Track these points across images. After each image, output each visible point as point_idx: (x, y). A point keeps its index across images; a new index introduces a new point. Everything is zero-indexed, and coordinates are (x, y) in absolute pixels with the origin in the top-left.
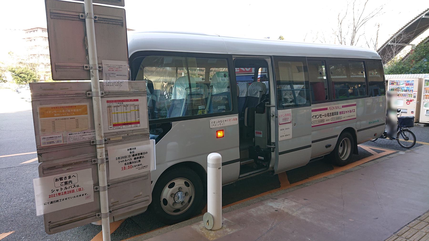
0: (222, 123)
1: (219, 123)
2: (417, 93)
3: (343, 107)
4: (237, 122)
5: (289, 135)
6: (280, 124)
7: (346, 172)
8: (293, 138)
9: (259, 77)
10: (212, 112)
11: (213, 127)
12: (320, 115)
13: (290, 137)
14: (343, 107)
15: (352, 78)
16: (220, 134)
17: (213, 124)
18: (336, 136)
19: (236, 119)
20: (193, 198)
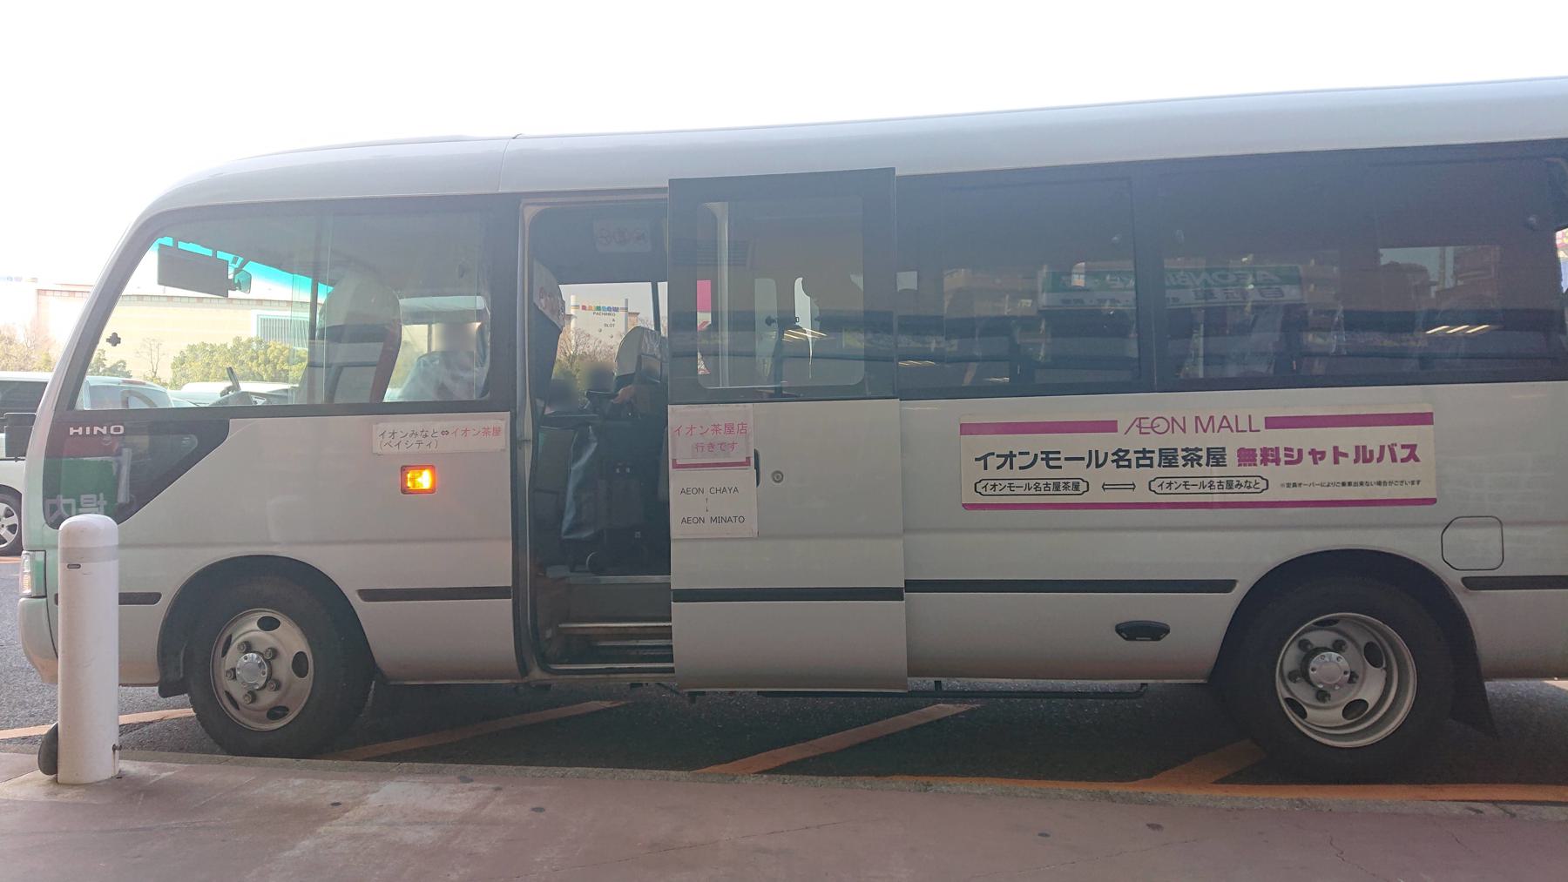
0: (426, 441)
1: (413, 440)
2: (1450, 251)
3: (1272, 423)
4: (502, 442)
5: (742, 519)
6: (676, 466)
7: (1110, 798)
8: (760, 536)
9: (1133, 335)
10: (339, 400)
11: (387, 450)
12: (1048, 457)
13: (752, 526)
14: (1272, 423)
15: (1394, 267)
16: (424, 480)
17: (387, 438)
18: (1226, 586)
19: (497, 431)
20: (220, 650)
